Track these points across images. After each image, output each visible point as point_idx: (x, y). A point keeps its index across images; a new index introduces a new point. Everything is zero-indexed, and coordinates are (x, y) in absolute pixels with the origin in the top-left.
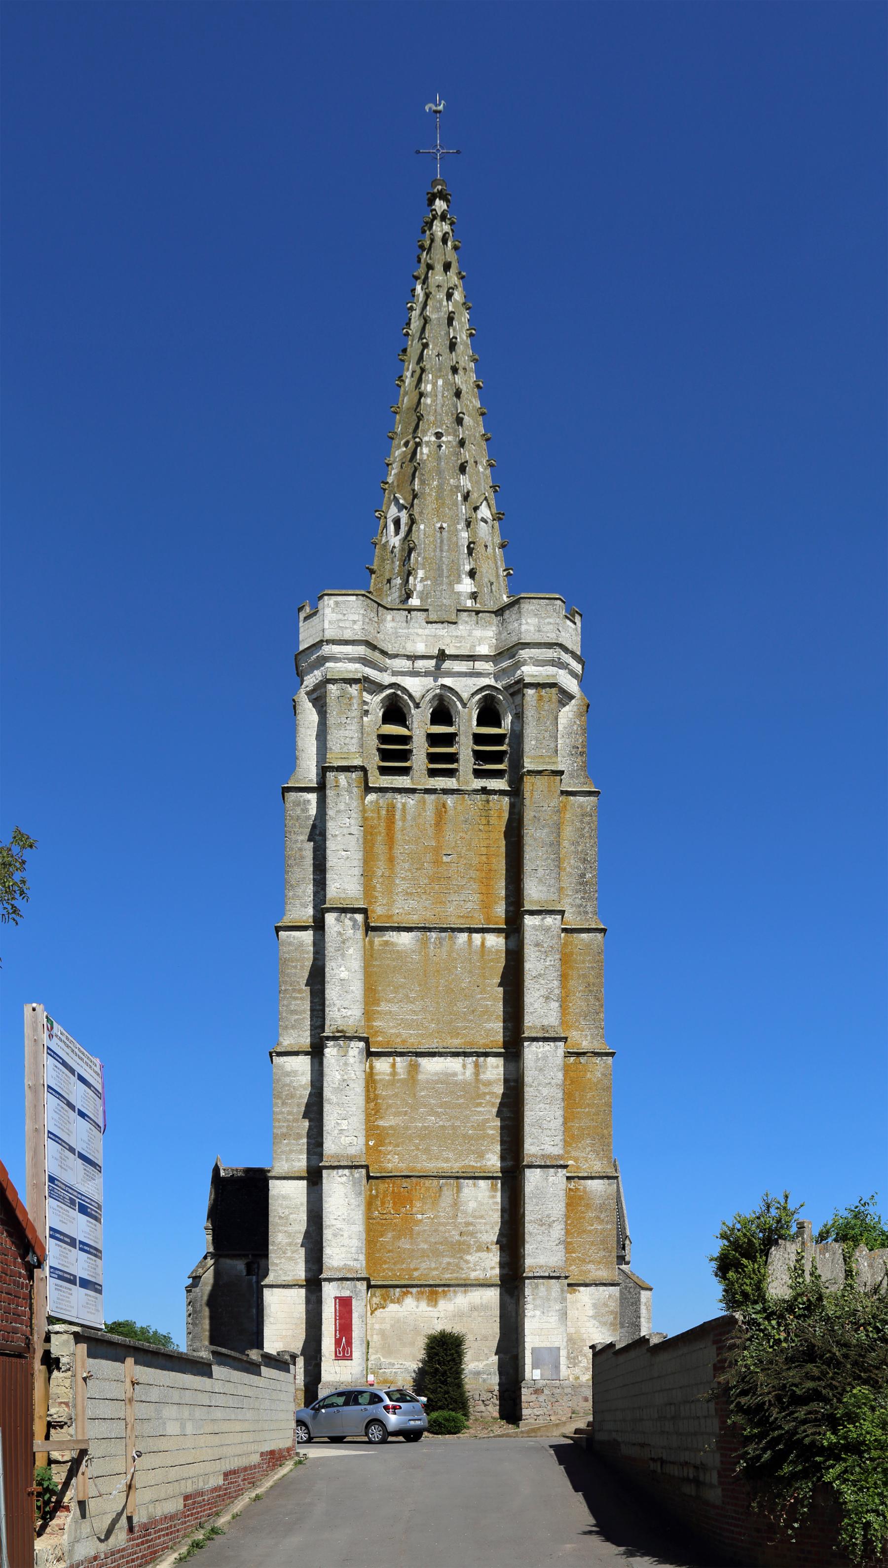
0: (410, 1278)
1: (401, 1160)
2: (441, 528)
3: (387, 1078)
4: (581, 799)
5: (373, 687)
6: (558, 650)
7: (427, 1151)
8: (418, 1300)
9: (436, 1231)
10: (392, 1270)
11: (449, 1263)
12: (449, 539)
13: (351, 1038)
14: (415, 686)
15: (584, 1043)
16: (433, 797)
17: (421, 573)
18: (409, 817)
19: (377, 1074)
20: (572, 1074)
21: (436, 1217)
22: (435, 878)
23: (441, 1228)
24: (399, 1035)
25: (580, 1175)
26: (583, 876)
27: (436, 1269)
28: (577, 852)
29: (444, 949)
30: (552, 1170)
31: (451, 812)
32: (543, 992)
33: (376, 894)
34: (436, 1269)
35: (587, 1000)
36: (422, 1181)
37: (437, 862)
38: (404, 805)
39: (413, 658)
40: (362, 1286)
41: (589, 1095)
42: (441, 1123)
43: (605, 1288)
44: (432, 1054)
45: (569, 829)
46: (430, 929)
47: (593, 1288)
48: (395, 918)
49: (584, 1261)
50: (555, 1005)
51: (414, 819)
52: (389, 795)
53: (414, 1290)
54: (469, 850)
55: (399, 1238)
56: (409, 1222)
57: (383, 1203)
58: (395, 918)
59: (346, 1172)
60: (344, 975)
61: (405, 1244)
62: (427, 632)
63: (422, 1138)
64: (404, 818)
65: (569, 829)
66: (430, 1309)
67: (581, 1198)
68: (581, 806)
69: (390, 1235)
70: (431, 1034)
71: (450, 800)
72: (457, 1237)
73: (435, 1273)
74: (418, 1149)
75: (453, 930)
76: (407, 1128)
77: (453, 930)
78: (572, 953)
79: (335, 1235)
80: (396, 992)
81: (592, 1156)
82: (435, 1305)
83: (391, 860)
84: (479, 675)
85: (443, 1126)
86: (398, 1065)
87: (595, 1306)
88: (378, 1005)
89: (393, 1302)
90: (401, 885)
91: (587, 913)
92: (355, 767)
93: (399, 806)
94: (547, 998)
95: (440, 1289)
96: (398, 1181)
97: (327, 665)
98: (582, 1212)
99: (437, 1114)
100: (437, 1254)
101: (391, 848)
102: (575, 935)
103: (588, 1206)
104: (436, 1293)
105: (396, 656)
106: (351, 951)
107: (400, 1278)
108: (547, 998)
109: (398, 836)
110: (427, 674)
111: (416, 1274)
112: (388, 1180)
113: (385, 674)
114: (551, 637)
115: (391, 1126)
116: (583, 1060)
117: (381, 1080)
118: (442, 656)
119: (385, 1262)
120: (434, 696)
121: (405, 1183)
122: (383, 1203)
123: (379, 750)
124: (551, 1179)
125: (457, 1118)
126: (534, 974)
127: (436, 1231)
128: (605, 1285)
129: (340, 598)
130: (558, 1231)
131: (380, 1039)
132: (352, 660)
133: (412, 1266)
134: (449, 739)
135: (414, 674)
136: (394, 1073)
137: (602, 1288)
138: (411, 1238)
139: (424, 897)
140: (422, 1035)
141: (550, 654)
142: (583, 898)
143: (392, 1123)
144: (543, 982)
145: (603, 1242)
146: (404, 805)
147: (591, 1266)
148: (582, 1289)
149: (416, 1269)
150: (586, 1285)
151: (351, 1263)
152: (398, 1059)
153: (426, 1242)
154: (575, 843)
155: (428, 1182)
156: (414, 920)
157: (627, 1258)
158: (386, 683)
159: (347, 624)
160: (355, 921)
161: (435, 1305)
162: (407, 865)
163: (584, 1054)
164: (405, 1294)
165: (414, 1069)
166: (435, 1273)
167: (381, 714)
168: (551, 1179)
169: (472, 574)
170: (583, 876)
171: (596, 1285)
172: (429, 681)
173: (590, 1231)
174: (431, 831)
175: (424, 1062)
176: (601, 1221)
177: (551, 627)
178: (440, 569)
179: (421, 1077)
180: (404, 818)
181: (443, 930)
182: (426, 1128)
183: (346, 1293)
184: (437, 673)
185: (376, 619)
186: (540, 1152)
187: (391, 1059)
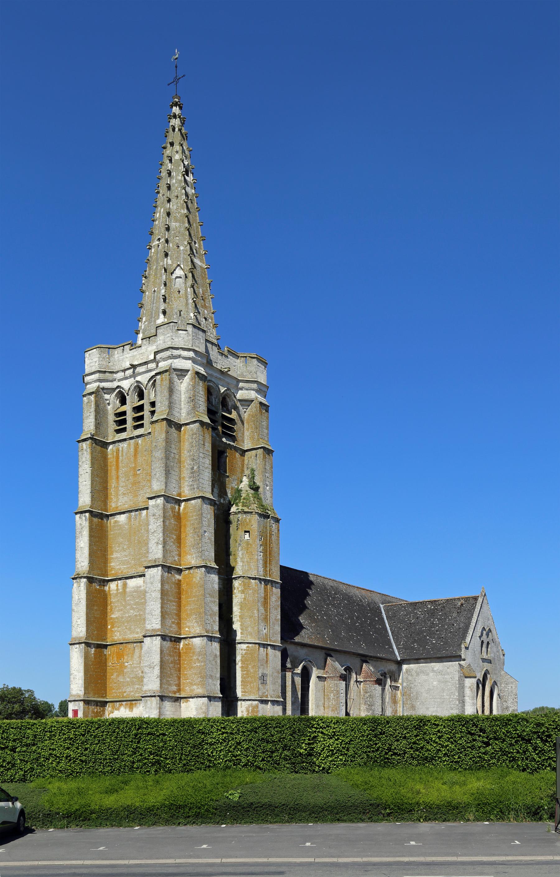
0: (123, 697)
1: (120, 635)
2: (154, 291)
3: (115, 592)
4: (192, 426)
5: (109, 391)
6: (171, 350)
7: (130, 629)
8: (125, 708)
9: (133, 671)
10: (116, 693)
11: (137, 688)
12: (157, 296)
13: (81, 578)
14: (126, 385)
15: (193, 562)
16: (133, 441)
17: (144, 319)
18: (124, 454)
19: (112, 591)
20: (187, 580)
21: (133, 664)
22: (134, 483)
23: (135, 670)
24: (120, 569)
25: (189, 636)
26: (193, 468)
27: (133, 691)
28: (190, 456)
29: (138, 520)
30: (154, 638)
31: (140, 447)
32: (156, 540)
33: (112, 497)
34: (133, 691)
35: (194, 537)
36: (127, 645)
37: (135, 475)
38: (122, 448)
39: (124, 371)
40: (81, 703)
41: (194, 591)
42: (135, 613)
43: (201, 699)
44: (131, 577)
45: (187, 444)
46: (131, 511)
47: (195, 699)
48: (119, 508)
49: (191, 684)
50: (160, 547)
51: (126, 454)
52: (117, 444)
53: (124, 703)
54: (147, 465)
55: (119, 676)
56: (122, 666)
57: (113, 658)
58: (119, 508)
59: (78, 646)
60: (82, 545)
61: (121, 679)
62: (130, 355)
63: (128, 622)
64: (122, 456)
65: (187, 444)
66: (130, 713)
67: (191, 649)
68: (192, 430)
69: (115, 675)
70: (132, 566)
71: (140, 441)
72: (141, 674)
73: (132, 693)
74: (126, 628)
75: (141, 509)
76: (122, 617)
77: (141, 509)
78: (188, 512)
79: (74, 678)
80: (119, 547)
81: (195, 625)
82: (132, 711)
83: (118, 478)
84: (150, 371)
85: (136, 615)
86: (119, 585)
87: (196, 709)
88: (113, 555)
89: (116, 710)
90: (122, 490)
91: (194, 489)
92: (87, 438)
93: (121, 449)
94: (157, 543)
95: (134, 702)
96: (118, 646)
97: (88, 386)
98: (191, 657)
99: (133, 609)
100: (133, 683)
101: (117, 472)
102: (189, 502)
103: (194, 653)
104: (131, 704)
105: (117, 372)
106: (85, 533)
107: (119, 697)
108: (157, 543)
109: (120, 465)
110: (131, 377)
111: (125, 694)
112: (115, 646)
113: (115, 382)
114: (169, 344)
115: (116, 617)
116: (192, 571)
117: (113, 594)
118: (133, 367)
119: (114, 689)
120: (135, 387)
121: (121, 647)
122: (113, 658)
123: (115, 421)
124: (154, 642)
125: (141, 610)
126: (152, 531)
127: (133, 671)
128: (200, 697)
129: (90, 352)
130: (157, 671)
131: (113, 572)
132: (95, 381)
133: (124, 691)
134: (124, 413)
135: (126, 378)
136: (117, 590)
137: (199, 699)
138: (123, 676)
139: (130, 494)
140: (128, 567)
141: (168, 353)
142: (193, 481)
143: (117, 616)
144: (156, 535)
145: (200, 673)
146: (122, 448)
147: (195, 687)
148: (191, 699)
149: (125, 692)
150: (192, 698)
151: (79, 692)
152: (119, 582)
153: (129, 677)
154: (189, 451)
155: (129, 646)
156: (126, 507)
157: (463, 657)
158: (115, 387)
159: (93, 364)
160: (85, 516)
161: (132, 711)
162: (123, 479)
163: (191, 568)
164: (121, 705)
165: (125, 585)
166: (132, 693)
167: (118, 402)
168: (154, 642)
169: (164, 313)
170: (193, 468)
171: (197, 697)
172: (132, 380)
173: (194, 667)
174: (132, 459)
175: (128, 581)
176: (199, 662)
177: (169, 338)
178: (152, 314)
179: (128, 590)
180: (122, 456)
181: (137, 510)
182: (129, 616)
183: (76, 708)
184: (134, 375)
185: (107, 356)
186: (152, 628)
187: (116, 582)
